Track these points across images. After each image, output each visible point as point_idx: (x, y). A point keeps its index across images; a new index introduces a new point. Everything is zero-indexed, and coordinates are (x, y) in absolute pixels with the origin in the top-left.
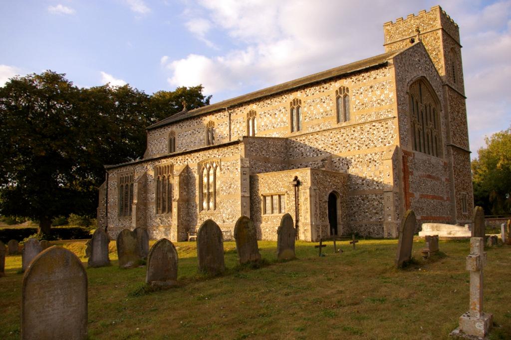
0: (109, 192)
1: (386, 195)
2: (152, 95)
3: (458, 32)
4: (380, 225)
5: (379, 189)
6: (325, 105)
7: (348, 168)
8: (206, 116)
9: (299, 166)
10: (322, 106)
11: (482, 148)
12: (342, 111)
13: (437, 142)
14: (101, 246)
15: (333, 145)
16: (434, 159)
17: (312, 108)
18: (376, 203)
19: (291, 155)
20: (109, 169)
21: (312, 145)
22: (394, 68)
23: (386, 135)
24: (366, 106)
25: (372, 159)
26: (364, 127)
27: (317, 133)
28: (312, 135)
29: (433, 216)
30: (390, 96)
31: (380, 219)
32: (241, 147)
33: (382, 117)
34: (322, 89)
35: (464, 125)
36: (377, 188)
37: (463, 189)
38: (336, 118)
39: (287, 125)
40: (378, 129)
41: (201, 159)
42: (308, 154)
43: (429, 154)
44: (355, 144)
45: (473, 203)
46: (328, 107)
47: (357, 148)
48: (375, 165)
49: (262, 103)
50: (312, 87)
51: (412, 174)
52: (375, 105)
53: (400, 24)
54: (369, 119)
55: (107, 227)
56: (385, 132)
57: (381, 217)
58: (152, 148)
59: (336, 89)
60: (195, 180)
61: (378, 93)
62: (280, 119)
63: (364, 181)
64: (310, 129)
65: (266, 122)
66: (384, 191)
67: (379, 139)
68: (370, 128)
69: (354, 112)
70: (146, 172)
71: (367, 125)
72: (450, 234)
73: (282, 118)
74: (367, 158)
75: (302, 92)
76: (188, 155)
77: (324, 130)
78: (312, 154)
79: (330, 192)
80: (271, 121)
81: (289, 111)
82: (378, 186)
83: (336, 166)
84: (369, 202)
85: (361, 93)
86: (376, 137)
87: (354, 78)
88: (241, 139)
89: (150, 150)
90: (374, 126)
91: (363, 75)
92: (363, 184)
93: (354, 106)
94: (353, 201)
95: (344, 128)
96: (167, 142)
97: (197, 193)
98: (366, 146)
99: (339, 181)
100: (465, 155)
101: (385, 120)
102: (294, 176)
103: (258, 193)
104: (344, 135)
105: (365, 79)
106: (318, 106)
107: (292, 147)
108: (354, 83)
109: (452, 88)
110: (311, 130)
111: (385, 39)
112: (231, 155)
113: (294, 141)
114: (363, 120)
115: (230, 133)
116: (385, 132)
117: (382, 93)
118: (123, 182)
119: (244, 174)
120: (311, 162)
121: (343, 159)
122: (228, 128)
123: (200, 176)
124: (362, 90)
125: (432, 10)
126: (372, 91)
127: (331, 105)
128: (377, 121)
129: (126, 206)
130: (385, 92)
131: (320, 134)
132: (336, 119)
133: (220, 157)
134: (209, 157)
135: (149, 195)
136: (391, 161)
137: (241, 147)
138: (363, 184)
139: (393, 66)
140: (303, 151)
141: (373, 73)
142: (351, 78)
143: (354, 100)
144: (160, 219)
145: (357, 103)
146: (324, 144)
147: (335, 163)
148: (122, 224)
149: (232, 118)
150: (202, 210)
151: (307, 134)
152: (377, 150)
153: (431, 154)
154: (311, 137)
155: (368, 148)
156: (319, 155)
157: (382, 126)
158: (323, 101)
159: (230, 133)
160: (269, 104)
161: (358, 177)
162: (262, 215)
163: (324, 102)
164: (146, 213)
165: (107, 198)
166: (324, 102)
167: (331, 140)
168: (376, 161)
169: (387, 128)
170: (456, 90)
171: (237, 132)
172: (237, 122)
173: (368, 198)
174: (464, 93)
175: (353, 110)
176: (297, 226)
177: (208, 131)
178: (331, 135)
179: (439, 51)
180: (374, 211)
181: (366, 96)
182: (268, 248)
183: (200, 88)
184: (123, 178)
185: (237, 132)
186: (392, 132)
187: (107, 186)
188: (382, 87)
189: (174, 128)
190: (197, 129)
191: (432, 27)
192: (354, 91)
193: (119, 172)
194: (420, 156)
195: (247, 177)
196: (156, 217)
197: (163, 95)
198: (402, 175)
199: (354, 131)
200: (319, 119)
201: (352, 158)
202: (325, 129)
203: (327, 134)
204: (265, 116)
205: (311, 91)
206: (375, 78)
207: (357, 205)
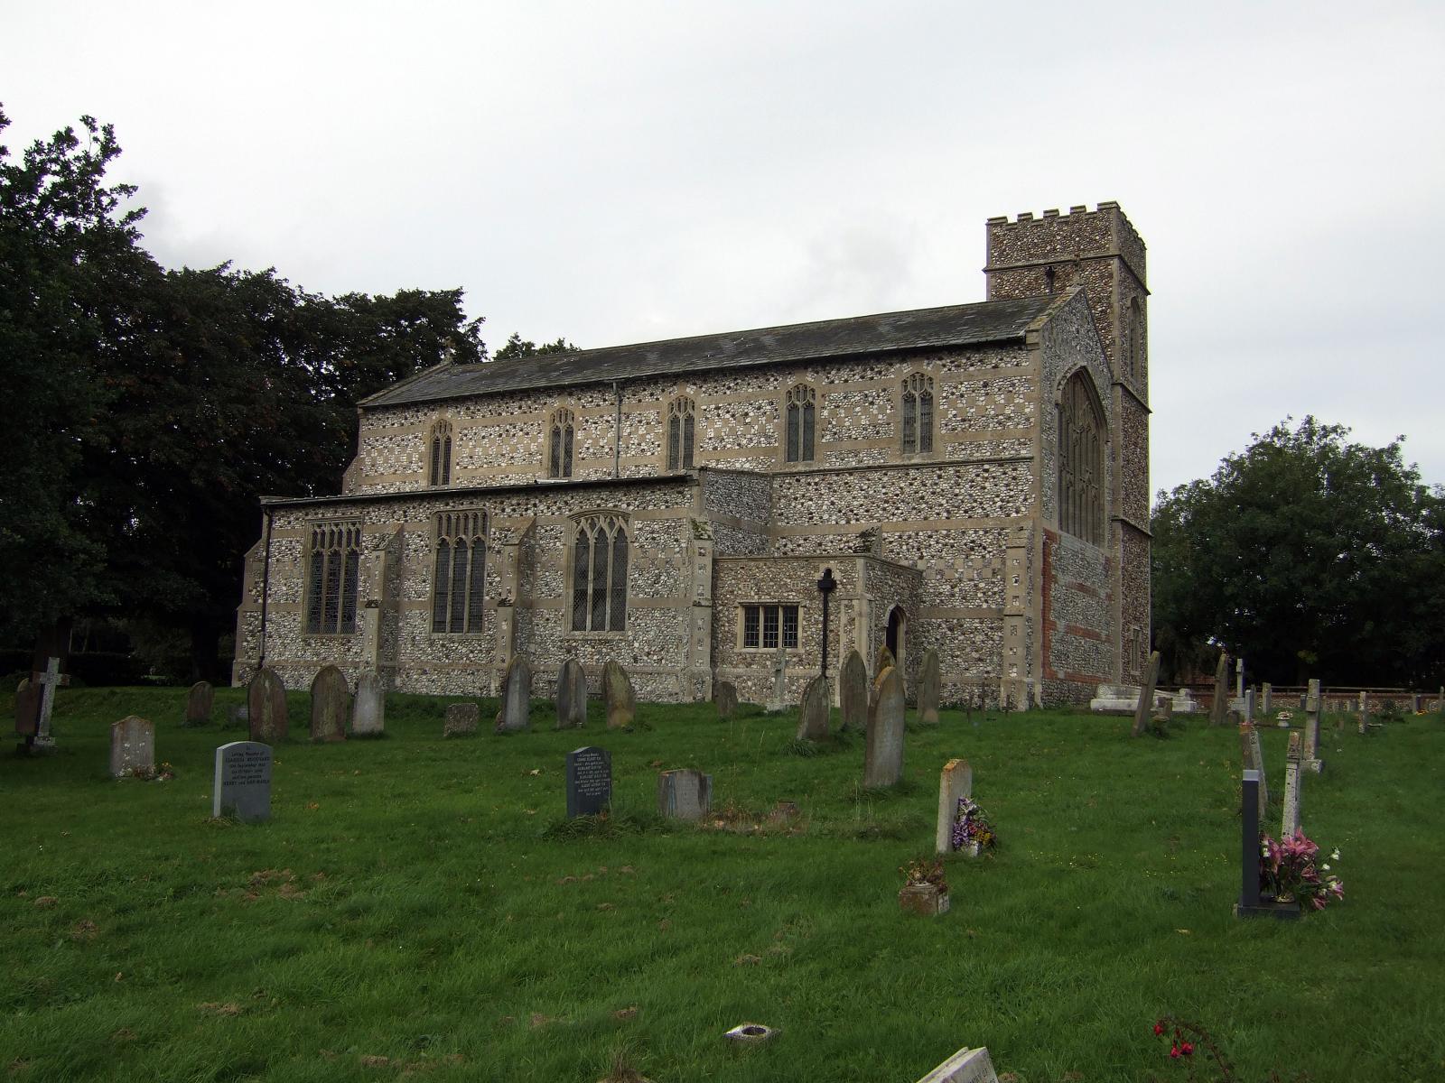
0: (271, 569)
2: (331, 299)
3: (1144, 257)
5: (989, 607)
9: (801, 542)
10: (865, 411)
11: (117, 156)
13: (1095, 512)
14: (520, 694)
15: (887, 502)
16: (1090, 550)
17: (842, 413)
18: (979, 638)
19: (781, 514)
20: (273, 508)
23: (1012, 493)
24: (970, 426)
26: (962, 470)
27: (851, 471)
28: (837, 475)
29: (1083, 673)
31: (987, 672)
33: (1006, 455)
35: (1144, 473)
36: (985, 606)
37: (1135, 618)
39: (777, 445)
40: (994, 478)
41: (576, 509)
42: (826, 517)
43: (1081, 537)
44: (942, 505)
45: (1149, 647)
46: (880, 417)
48: (983, 557)
51: (1056, 582)
54: (977, 455)
55: (262, 658)
56: (1011, 487)
57: (989, 669)
58: (374, 459)
61: (1001, 399)
62: (756, 427)
63: (957, 590)
66: (1005, 613)
67: (997, 499)
68: (978, 475)
69: (944, 435)
71: (970, 468)
73: (763, 427)
74: (967, 539)
77: (869, 467)
79: (892, 607)
80: (733, 431)
81: (783, 412)
83: (892, 551)
84: (964, 634)
85: (962, 396)
89: (368, 461)
90: (986, 471)
92: (953, 595)
94: (928, 631)
95: (917, 467)
99: (905, 585)
100: (1141, 542)
101: (1014, 461)
105: (972, 365)
106: (858, 409)
107: (785, 497)
109: (1130, 392)
110: (838, 465)
112: (663, 507)
116: (1011, 487)
117: (1008, 402)
118: (340, 544)
120: (831, 537)
126: (987, 394)
127: (888, 411)
128: (995, 460)
129: (332, 606)
134: (599, 505)
138: (953, 595)
142: (940, 359)
143: (946, 412)
145: (950, 416)
146: (865, 497)
147: (891, 543)
148: (318, 655)
152: (990, 523)
153: (1084, 538)
155: (970, 517)
156: (853, 522)
157: (1005, 473)
158: (870, 399)
165: (265, 582)
166: (872, 403)
167: (884, 491)
168: (985, 548)
169: (1014, 478)
170: (1135, 393)
173: (962, 626)
174: (1147, 402)
175: (940, 431)
178: (885, 479)
179: (1110, 306)
180: (975, 655)
181: (972, 404)
183: (458, 293)
184: (323, 534)
185: (639, 444)
187: (268, 552)
188: (1011, 389)
190: (519, 425)
191: (1099, 248)
193: (309, 517)
194: (1069, 541)
197: (358, 303)
198: (1039, 581)
199: (940, 477)
200: (856, 439)
203: (876, 475)
204: (719, 415)
206: (996, 367)
207: (937, 639)
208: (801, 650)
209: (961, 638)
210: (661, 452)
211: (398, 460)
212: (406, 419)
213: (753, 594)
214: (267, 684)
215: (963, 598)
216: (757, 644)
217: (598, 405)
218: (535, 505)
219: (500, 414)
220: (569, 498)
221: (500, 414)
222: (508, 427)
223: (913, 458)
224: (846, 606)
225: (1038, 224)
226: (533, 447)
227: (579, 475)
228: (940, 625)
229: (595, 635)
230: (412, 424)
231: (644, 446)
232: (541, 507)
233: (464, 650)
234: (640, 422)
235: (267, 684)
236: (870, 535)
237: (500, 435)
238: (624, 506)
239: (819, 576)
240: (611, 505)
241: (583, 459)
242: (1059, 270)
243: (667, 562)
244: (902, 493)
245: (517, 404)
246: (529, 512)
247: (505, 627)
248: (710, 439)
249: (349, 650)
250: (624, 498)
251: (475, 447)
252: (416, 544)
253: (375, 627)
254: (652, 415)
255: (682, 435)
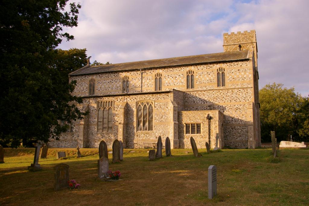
1: (250, 127)
4: (242, 142)
6: (210, 76)
7: (224, 112)
8: (122, 73)
9: (192, 108)
10: (208, 76)
12: (221, 80)
15: (214, 98)
17: (201, 77)
18: (240, 131)
21: (201, 97)
22: (252, 62)
23: (247, 96)
24: (235, 80)
25: (238, 108)
26: (234, 90)
27: (204, 91)
28: (201, 92)
30: (250, 76)
31: (242, 139)
32: (171, 95)
33: (245, 87)
34: (208, 67)
36: (241, 123)
38: (217, 84)
39: (184, 84)
41: (138, 100)
42: (198, 102)
47: (230, 101)
48: (240, 111)
49: (166, 70)
50: (201, 65)
52: (241, 80)
53: (233, 36)
54: (237, 87)
57: (243, 138)
59: (217, 68)
60: (133, 112)
61: (243, 74)
63: (233, 119)
64: (200, 88)
65: (169, 81)
67: (243, 97)
70: (88, 105)
71: (235, 90)
72: (296, 146)
74: (235, 107)
75: (195, 67)
76: (127, 96)
78: (200, 102)
80: (172, 81)
81: (186, 77)
82: (241, 122)
85: (233, 73)
86: (240, 97)
87: (228, 64)
88: (172, 90)
90: (240, 91)
91: (234, 63)
93: (228, 79)
95: (222, 90)
96: (87, 86)
97: (135, 120)
98: (235, 100)
102: (207, 114)
103: (182, 122)
104: (222, 94)
105: (235, 65)
106: (206, 76)
107: (187, 97)
108: (228, 66)
110: (201, 89)
111: (224, 42)
112: (163, 99)
113: (188, 94)
114: (233, 87)
115: (142, 85)
117: (245, 74)
119: (175, 111)
120: (200, 107)
121: (221, 107)
122: (140, 82)
123: (137, 110)
124: (233, 71)
125: (251, 32)
128: (242, 88)
130: (247, 74)
131: (206, 91)
132: (217, 85)
133: (154, 99)
134: (145, 99)
135: (91, 119)
136: (252, 109)
137: (171, 95)
138: (232, 121)
139: (252, 61)
140: (195, 100)
141: (240, 63)
143: (228, 77)
144: (101, 135)
145: (230, 77)
148: (64, 138)
149: (143, 76)
150: (138, 130)
151: (198, 91)
152: (241, 103)
154: (200, 92)
157: (245, 91)
158: (209, 74)
159: (142, 85)
160: (171, 71)
161: (229, 116)
162: (185, 134)
163: (209, 74)
164: (88, 131)
166: (209, 74)
167: (213, 95)
168: (240, 109)
169: (247, 92)
171: (147, 85)
172: (147, 79)
173: (235, 128)
175: (227, 81)
176: (217, 139)
177: (124, 81)
178: (214, 93)
182: (80, 161)
183: (85, 50)
185: (147, 85)
186: (250, 95)
189: (94, 77)
190: (114, 80)
192: (228, 71)
195: (177, 112)
196: (97, 134)
199: (228, 92)
201: (226, 106)
202: (210, 89)
203: (211, 92)
204: (169, 77)
205: (201, 67)
206: (241, 66)
207: (229, 131)
208: (202, 134)
209: (235, 131)
210: (154, 86)
211: (80, 89)
212: (82, 78)
213: (188, 120)
214: (103, 145)
215: (235, 121)
216: (190, 133)
217: (136, 75)
218: (127, 99)
219: (109, 77)
220: (136, 97)
221: (109, 77)
222: (111, 80)
223: (220, 87)
224: (214, 123)
225: (236, 35)
226: (118, 85)
227: (163, 90)
228: (229, 128)
229: (144, 131)
230: (84, 80)
231: (148, 85)
232: (128, 99)
233: (107, 136)
234: (147, 79)
235: (103, 145)
236: (211, 106)
237: (109, 82)
238: (152, 99)
239: (206, 116)
240: (148, 99)
241: (132, 88)
242: (242, 45)
243: (165, 113)
244: (218, 96)
245: (113, 75)
246: (125, 100)
247: (121, 130)
248: (166, 83)
249: (73, 137)
250: (152, 97)
251: (102, 85)
252: (92, 109)
253: (83, 130)
254: (151, 78)
255: (158, 81)
